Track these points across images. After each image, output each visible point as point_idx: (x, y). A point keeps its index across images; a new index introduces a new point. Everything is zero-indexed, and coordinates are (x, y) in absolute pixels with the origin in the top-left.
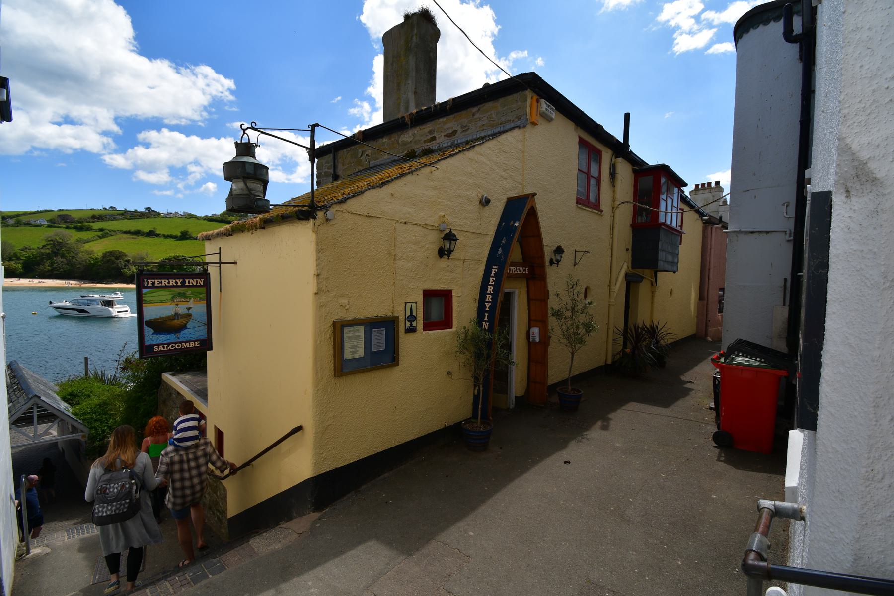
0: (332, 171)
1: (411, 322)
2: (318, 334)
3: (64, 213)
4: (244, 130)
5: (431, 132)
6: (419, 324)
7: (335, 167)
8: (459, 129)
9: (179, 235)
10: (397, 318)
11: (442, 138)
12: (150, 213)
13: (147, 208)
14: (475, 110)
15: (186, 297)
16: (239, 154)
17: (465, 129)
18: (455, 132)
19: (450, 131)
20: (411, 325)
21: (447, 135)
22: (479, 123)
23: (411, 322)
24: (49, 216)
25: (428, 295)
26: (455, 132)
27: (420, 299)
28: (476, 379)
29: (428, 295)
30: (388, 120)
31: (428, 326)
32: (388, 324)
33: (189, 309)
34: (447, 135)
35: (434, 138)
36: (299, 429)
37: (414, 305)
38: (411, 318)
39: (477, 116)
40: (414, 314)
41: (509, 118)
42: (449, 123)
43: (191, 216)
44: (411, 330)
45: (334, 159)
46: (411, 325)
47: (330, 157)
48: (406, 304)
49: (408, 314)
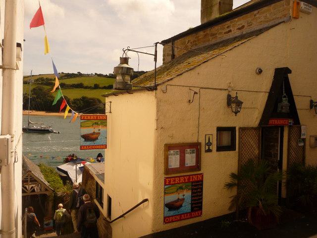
0: (171, 52)
1: (209, 146)
2: (156, 151)
3: (42, 76)
4: (124, 51)
5: (228, 27)
6: (214, 147)
7: (173, 50)
8: (246, 25)
9: (93, 86)
10: (200, 143)
11: (235, 31)
12: (80, 75)
13: (78, 73)
14: (256, 12)
15: (98, 125)
16: (122, 63)
17: (250, 25)
18: (243, 27)
19: (241, 26)
20: (209, 148)
21: (239, 29)
22: (259, 20)
23: (209, 146)
24: (36, 78)
25: (220, 130)
26: (243, 27)
27: (215, 132)
28: (155, 204)
29: (220, 130)
30: (203, 23)
31: (220, 149)
32: (195, 147)
33: (99, 130)
34: (239, 29)
35: (230, 31)
36: (146, 200)
37: (211, 137)
38: (209, 144)
39: (257, 16)
40: (211, 141)
41: (278, 16)
42: (240, 21)
43: (100, 75)
44: (209, 151)
45: (173, 44)
46: (209, 148)
47: (170, 44)
48: (206, 135)
49: (207, 141)
